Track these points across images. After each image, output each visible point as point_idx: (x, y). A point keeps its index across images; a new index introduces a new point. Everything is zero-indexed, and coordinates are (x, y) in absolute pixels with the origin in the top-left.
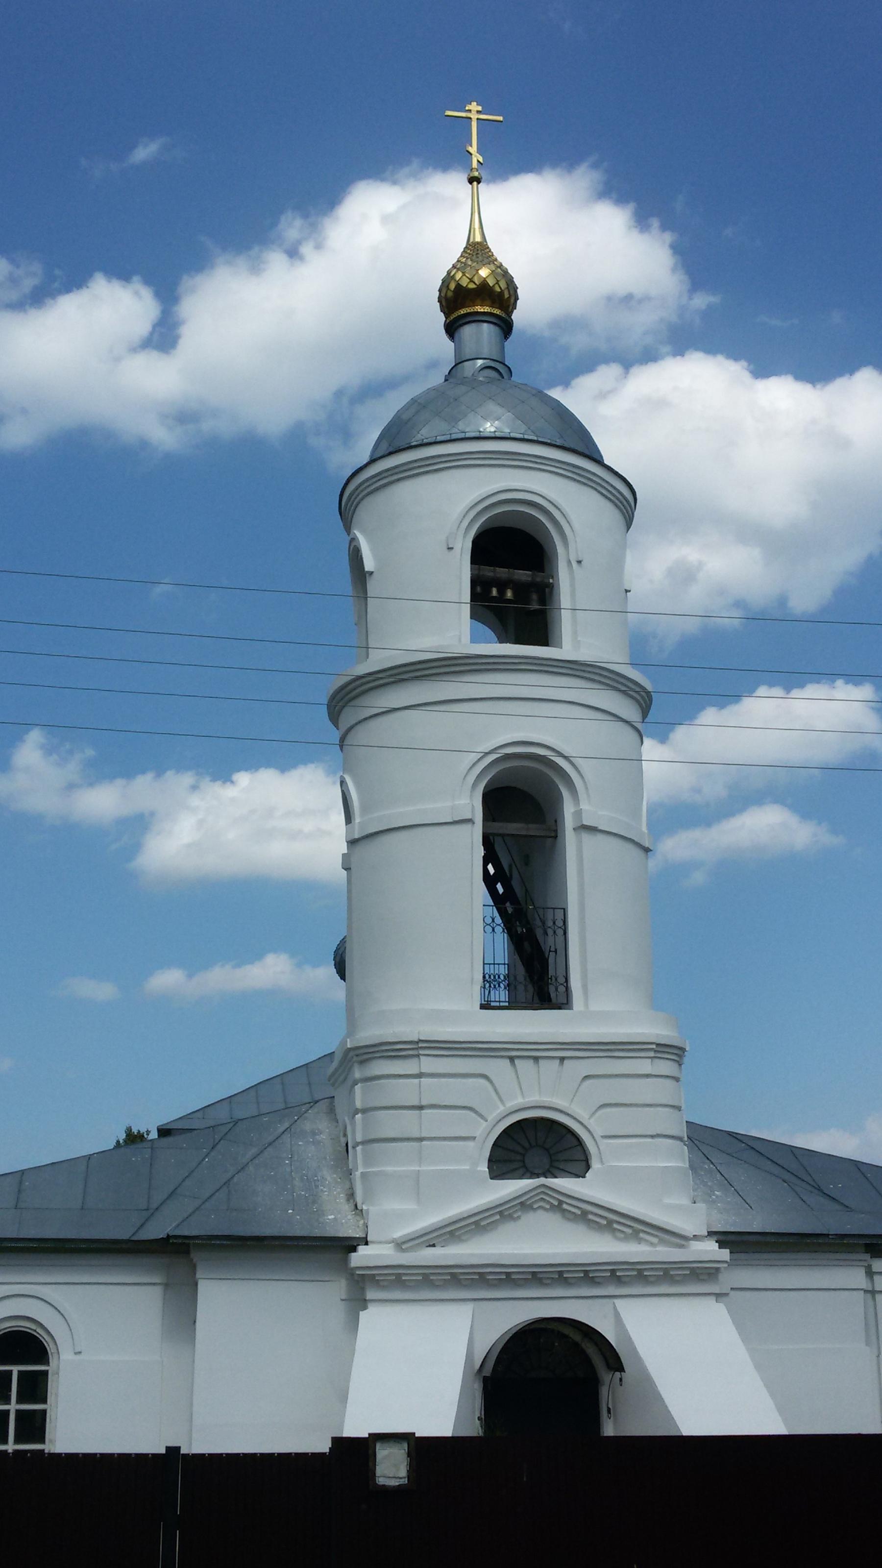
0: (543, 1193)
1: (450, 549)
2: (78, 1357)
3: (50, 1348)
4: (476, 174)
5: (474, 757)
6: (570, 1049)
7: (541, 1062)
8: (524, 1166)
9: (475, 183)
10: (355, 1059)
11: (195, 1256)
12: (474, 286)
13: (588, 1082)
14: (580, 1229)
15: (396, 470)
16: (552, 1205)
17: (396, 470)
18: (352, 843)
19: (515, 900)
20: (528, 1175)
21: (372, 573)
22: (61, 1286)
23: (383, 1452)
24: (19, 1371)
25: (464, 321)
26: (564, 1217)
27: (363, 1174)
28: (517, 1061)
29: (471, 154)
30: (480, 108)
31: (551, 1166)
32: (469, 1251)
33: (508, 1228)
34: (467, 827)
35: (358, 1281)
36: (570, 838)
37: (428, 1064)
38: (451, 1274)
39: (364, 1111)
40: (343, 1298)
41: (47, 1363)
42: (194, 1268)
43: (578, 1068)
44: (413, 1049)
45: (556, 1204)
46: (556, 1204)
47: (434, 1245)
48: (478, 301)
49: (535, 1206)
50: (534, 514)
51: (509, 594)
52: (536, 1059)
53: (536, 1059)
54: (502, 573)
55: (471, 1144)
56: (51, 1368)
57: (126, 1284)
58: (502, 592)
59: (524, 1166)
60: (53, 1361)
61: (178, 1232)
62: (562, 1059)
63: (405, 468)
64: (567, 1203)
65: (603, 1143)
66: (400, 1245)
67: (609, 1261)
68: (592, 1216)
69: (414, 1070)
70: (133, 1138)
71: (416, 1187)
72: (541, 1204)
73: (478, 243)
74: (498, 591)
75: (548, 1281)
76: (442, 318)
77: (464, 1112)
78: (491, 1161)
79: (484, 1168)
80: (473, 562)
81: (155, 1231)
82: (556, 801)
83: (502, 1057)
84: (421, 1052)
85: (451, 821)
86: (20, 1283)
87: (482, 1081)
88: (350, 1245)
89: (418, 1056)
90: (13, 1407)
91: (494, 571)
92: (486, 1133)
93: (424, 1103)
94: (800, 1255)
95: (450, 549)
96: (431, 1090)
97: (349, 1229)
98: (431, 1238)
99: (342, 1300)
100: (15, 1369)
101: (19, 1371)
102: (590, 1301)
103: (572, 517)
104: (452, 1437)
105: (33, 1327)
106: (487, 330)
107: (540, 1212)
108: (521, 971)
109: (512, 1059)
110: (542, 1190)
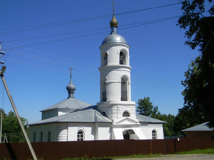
24: (81, 137)
56: (83, 134)
66: (116, 123)
78: (123, 115)
98: (119, 122)
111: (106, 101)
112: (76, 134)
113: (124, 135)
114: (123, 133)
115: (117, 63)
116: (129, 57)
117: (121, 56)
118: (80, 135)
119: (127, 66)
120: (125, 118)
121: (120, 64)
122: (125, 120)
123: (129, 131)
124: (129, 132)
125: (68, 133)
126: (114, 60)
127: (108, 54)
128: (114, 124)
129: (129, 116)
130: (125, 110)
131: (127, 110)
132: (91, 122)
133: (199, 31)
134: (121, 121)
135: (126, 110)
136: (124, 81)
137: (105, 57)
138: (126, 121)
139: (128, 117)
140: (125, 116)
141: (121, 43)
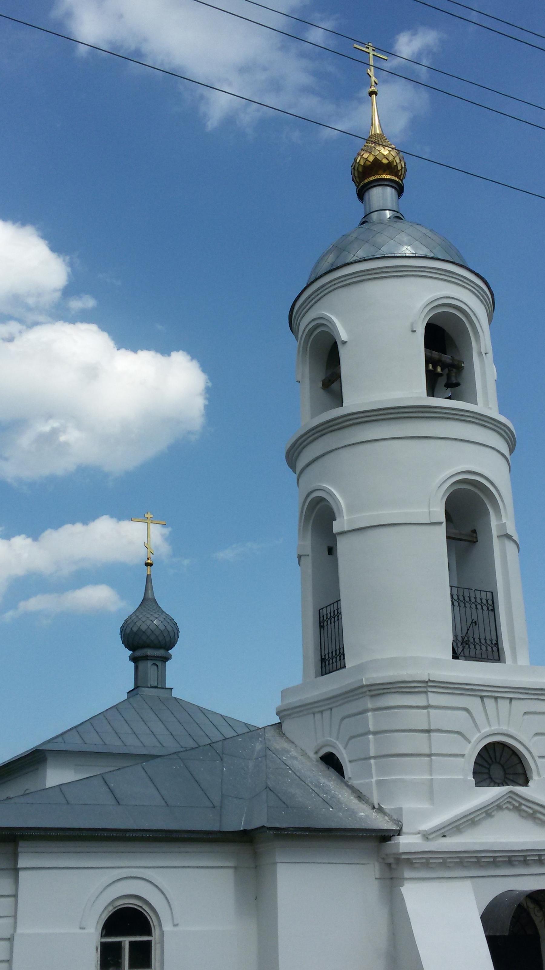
0: (510, 797)
1: (414, 331)
2: (176, 929)
3: (153, 922)
4: (373, 89)
6: (518, 693)
7: (499, 701)
8: (491, 778)
9: (374, 95)
10: (368, 693)
12: (370, 163)
13: (346, 721)
14: (529, 825)
15: (369, 272)
16: (513, 805)
17: (369, 272)
20: (492, 784)
21: (346, 342)
22: (188, 870)
24: (131, 943)
25: (372, 185)
26: (521, 816)
27: (379, 782)
28: (485, 700)
29: (370, 76)
31: (505, 777)
32: (456, 841)
33: (487, 824)
35: (389, 865)
37: (434, 699)
38: (460, 858)
39: (375, 733)
40: (377, 876)
41: (149, 933)
42: (15, 857)
43: (520, 707)
44: (424, 687)
45: (517, 805)
46: (517, 805)
47: (444, 836)
48: (380, 172)
49: (504, 807)
50: (461, 317)
52: (496, 698)
53: (496, 698)
55: (461, 760)
56: (154, 938)
57: (60, 868)
59: (491, 778)
60: (156, 932)
62: (511, 699)
63: (378, 271)
64: (524, 805)
65: (540, 761)
66: (426, 836)
67: (502, 849)
68: (534, 814)
69: (424, 703)
71: (431, 792)
72: (508, 805)
73: (376, 135)
74: (433, 367)
75: (517, 863)
77: (456, 735)
78: (475, 773)
79: (471, 778)
83: (476, 696)
84: (430, 689)
85: (429, 522)
86: (134, 867)
87: (465, 713)
88: (384, 837)
89: (426, 692)
91: (431, 353)
92: (472, 750)
93: (432, 727)
95: (414, 331)
96: (439, 719)
97: (382, 823)
98: (444, 831)
99: (376, 879)
101: (131, 943)
102: (538, 878)
105: (140, 904)
106: (390, 192)
107: (506, 812)
109: (482, 697)
110: (510, 795)
111: (345, 667)
112: (91, 937)
113: (492, 941)
114: (488, 918)
115: (411, 386)
116: (492, 372)
117: (435, 355)
118: (126, 941)
119: (479, 408)
120: (492, 793)
121: (431, 391)
122: (487, 812)
123: (531, 906)
124: (537, 917)
125: (160, 688)
126: (387, 366)
127: (343, 334)
128: (407, 842)
129: (526, 783)
130: (486, 730)
131: (504, 728)
132: (216, 828)
133: (406, 247)
134: (470, 821)
135: (495, 728)
136: (465, 515)
137: (327, 358)
138: (508, 818)
139: (519, 789)
140: (493, 782)
141: (425, 257)
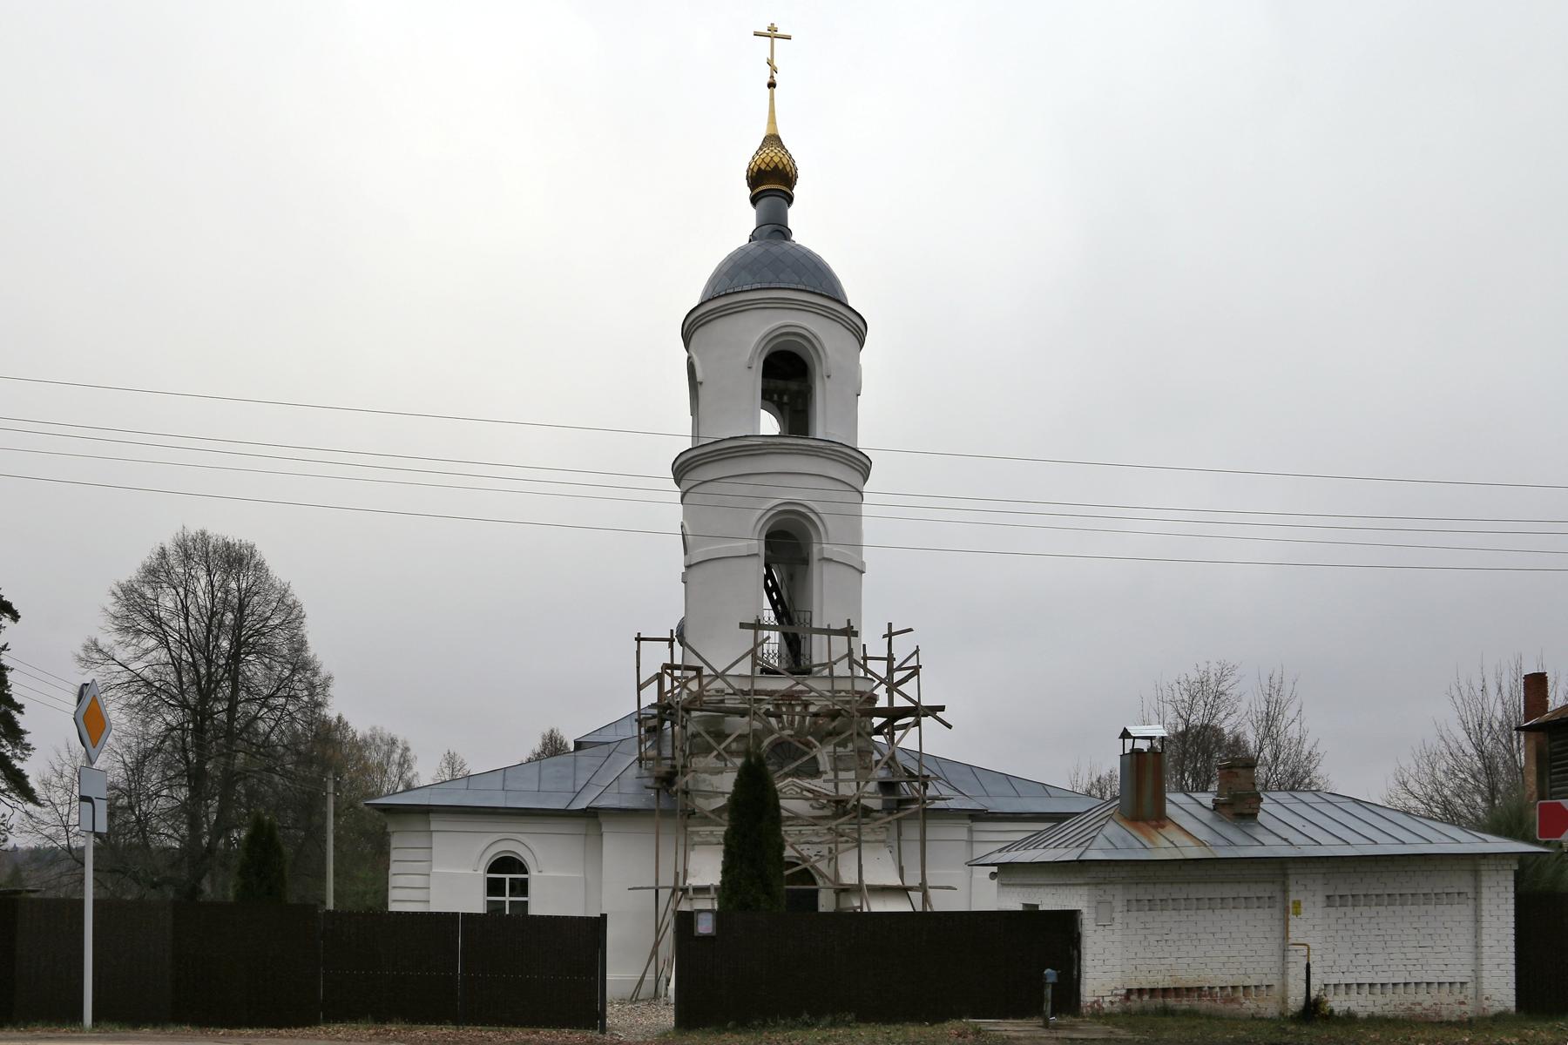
5: (759, 513)
11: (601, 819)
18: (688, 567)
19: (783, 606)
23: (701, 917)
30: (705, 926)
34: (755, 560)
36: (816, 567)
42: (600, 825)
51: (785, 399)
54: (780, 384)
58: (780, 397)
61: (595, 804)
70: (553, 747)
76: (749, 192)
80: (764, 376)
81: (581, 804)
82: (809, 544)
90: (507, 899)
94: (1211, 904)
100: (507, 877)
103: (826, 346)
104: (727, 853)
108: (785, 649)
